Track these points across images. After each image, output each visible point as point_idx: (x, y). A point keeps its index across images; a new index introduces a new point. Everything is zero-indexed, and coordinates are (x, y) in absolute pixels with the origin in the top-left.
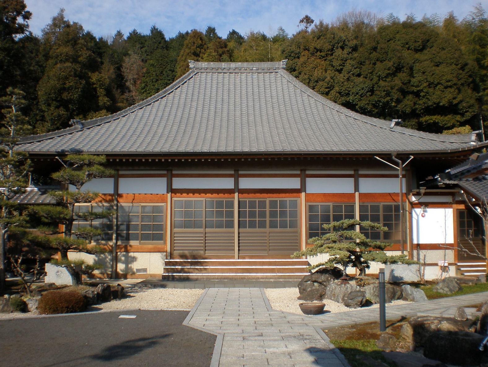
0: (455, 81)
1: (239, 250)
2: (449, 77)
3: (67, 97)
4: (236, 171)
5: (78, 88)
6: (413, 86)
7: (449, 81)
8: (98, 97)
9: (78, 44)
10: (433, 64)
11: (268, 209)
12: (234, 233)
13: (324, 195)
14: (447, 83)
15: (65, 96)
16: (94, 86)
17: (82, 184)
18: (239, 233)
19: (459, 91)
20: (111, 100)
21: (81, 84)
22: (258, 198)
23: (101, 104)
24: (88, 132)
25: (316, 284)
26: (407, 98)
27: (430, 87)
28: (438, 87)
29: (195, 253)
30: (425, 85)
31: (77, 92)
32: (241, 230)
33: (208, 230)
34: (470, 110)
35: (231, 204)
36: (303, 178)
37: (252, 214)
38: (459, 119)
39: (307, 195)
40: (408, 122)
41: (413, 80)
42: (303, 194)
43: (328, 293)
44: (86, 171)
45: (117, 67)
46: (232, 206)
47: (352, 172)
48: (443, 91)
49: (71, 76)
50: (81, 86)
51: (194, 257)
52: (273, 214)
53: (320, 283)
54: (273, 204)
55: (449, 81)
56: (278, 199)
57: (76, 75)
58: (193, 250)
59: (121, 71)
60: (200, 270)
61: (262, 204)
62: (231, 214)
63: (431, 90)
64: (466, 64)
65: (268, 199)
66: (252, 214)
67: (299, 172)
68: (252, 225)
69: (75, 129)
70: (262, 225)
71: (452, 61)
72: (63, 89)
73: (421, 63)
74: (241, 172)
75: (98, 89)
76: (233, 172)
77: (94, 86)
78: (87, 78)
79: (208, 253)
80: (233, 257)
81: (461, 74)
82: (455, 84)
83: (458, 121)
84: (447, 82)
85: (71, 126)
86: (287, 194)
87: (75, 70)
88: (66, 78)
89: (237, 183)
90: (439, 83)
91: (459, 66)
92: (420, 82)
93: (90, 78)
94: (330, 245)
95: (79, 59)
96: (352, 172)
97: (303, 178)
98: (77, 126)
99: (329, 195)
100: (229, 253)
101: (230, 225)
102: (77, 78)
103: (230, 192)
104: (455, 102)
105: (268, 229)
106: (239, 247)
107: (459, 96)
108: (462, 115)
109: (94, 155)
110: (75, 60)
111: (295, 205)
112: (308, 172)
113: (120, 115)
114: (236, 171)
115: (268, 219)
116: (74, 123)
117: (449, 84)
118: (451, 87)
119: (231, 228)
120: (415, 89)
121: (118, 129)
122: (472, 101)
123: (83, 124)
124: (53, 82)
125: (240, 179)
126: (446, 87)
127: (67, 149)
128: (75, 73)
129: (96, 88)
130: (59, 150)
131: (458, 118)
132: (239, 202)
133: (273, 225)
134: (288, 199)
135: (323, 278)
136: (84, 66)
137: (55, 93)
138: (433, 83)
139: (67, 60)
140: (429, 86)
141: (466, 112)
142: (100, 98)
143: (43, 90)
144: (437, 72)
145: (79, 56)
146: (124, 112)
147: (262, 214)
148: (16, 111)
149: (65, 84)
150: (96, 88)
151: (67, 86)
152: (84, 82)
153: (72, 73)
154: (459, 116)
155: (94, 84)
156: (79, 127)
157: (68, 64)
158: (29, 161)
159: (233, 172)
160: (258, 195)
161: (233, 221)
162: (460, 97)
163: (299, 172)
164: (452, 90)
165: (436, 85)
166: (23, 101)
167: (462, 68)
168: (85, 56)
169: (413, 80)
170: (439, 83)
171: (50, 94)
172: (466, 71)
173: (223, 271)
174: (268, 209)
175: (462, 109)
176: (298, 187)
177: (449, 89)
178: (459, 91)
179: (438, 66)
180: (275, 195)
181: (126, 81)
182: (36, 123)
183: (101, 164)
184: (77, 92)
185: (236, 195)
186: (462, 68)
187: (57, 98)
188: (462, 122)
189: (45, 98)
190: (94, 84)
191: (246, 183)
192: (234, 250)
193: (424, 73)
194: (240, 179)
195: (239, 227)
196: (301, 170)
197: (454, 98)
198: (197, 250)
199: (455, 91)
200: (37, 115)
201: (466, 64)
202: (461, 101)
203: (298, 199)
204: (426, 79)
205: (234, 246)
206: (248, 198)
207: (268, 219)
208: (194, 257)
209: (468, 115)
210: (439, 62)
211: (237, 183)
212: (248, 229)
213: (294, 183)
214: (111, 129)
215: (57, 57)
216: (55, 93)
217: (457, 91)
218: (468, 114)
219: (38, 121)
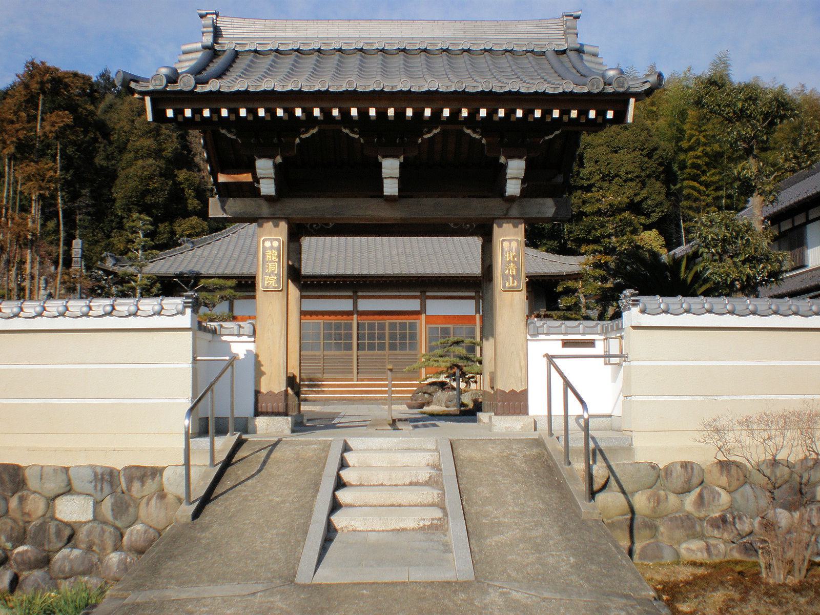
0: (637, 171)
1: (358, 373)
2: (630, 167)
3: (151, 200)
4: (355, 292)
5: (164, 191)
6: (582, 179)
7: (629, 173)
8: (187, 199)
9: (162, 134)
10: (609, 149)
11: (387, 332)
12: (352, 355)
13: (445, 317)
14: (627, 176)
15: (149, 199)
16: (182, 186)
17: (214, 306)
18: (358, 356)
19: (644, 184)
20: (202, 203)
21: (167, 184)
22: (377, 320)
23: (190, 208)
24: (199, 251)
25: (426, 395)
26: (574, 194)
27: (604, 181)
28: (615, 180)
29: (312, 376)
30: (598, 177)
31: (163, 195)
32: (360, 352)
33: (325, 353)
34: (657, 210)
35: (349, 327)
36: (424, 299)
37: (371, 337)
38: (643, 222)
39: (427, 317)
40: (576, 225)
41: (583, 171)
42: (423, 316)
43: (434, 400)
44: (218, 295)
45: (181, 135)
46: (351, 339)
47: (473, 294)
48: (621, 186)
49: (155, 175)
50: (168, 188)
51: (311, 380)
52: (393, 337)
53: (430, 394)
54: (393, 326)
55: (629, 173)
56: (407, 321)
57: (161, 175)
58: (310, 373)
59: (186, 140)
60: (318, 392)
61: (382, 327)
62: (349, 337)
63: (605, 184)
64: (655, 149)
65: (388, 321)
66: (371, 337)
67: (419, 294)
68: (371, 347)
69: (186, 248)
70: (382, 347)
71: (636, 145)
72: (146, 192)
73: (594, 148)
74: (359, 294)
75: (186, 190)
76: (351, 294)
77: (182, 186)
78: (173, 177)
79: (326, 376)
80: (352, 380)
81: (646, 163)
82: (637, 177)
83: (641, 224)
84: (627, 173)
85: (180, 245)
86: (407, 316)
87: (160, 167)
88: (150, 178)
89: (355, 305)
90: (616, 176)
91: (645, 152)
92: (591, 174)
93: (176, 176)
94: (436, 359)
95: (164, 154)
96: (473, 294)
97: (424, 299)
98: (187, 244)
99: (449, 317)
100: (349, 376)
101: (349, 347)
102: (163, 178)
103: (349, 313)
104: (637, 199)
105: (387, 352)
106: (358, 369)
107: (642, 192)
108: (648, 216)
109: (220, 277)
110: (157, 153)
111: (413, 326)
112: (428, 294)
113: (229, 231)
114: (355, 292)
115: (387, 341)
116: (184, 241)
117: (630, 176)
118: (632, 180)
119: (348, 373)
120: (585, 183)
121: (231, 248)
122: (662, 198)
123: (193, 243)
124: (132, 184)
125: (359, 300)
126: (626, 181)
127: (184, 271)
128: (160, 172)
129: (183, 189)
130: (178, 272)
131: (643, 219)
132: (358, 324)
133: (393, 347)
134: (407, 320)
135: (432, 389)
136: (168, 161)
137: (137, 196)
138: (608, 175)
139: (149, 156)
140: (603, 179)
141: (653, 212)
142: (190, 201)
143: (121, 191)
144: (615, 160)
145: (164, 150)
146: (234, 228)
147: (382, 337)
148: (144, 236)
149: (148, 185)
150: (183, 189)
151: (151, 187)
152: (171, 183)
153: (158, 172)
154: (644, 217)
155: (182, 184)
156: (190, 245)
157: (151, 161)
158: (158, 285)
159: (351, 294)
160: (377, 317)
161: (352, 343)
162: (643, 194)
163: (419, 294)
164: (634, 184)
165: (613, 178)
166: (150, 227)
167: (649, 156)
168: (170, 150)
169: (583, 171)
170: (616, 176)
171: (130, 197)
172: (655, 157)
173: (342, 392)
174: (387, 332)
175: (646, 209)
176: (418, 309)
177: (630, 183)
178: (644, 184)
179: (616, 152)
180: (394, 317)
181: (194, 155)
182: (111, 232)
183: (231, 288)
184: (163, 195)
185: (355, 316)
186: (649, 156)
187: (139, 201)
188: (648, 225)
189: (124, 201)
190: (181, 183)
191: (365, 305)
192: (352, 373)
193: (596, 162)
194: (359, 300)
195: (358, 350)
196: (421, 292)
197: (636, 195)
198: (314, 373)
199: (637, 185)
200: (112, 221)
201: (655, 149)
202: (645, 199)
203: (418, 321)
204: (600, 170)
205: (352, 369)
206: (366, 321)
207: (387, 341)
208: (311, 380)
209: (655, 217)
210: (618, 147)
211: (355, 305)
212: (366, 352)
213: (414, 305)
214: (224, 248)
215: (137, 151)
216: (137, 196)
217: (639, 185)
218: (654, 215)
219: (114, 229)
